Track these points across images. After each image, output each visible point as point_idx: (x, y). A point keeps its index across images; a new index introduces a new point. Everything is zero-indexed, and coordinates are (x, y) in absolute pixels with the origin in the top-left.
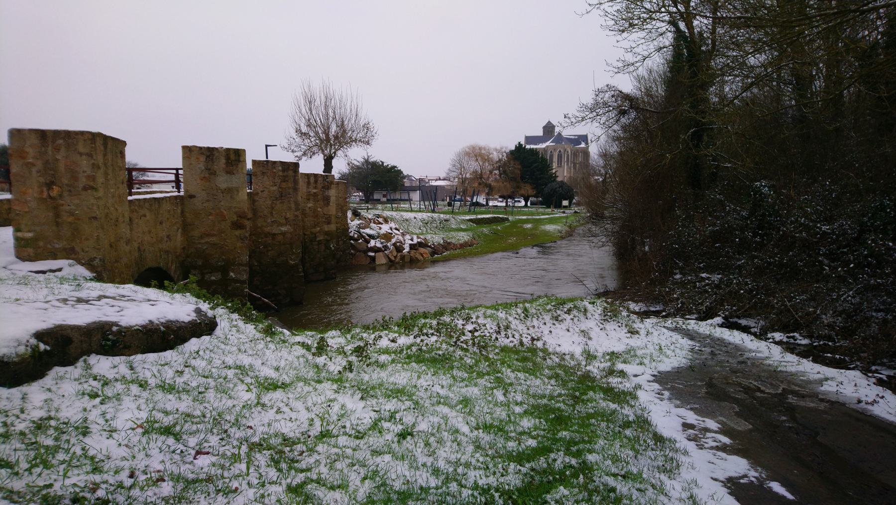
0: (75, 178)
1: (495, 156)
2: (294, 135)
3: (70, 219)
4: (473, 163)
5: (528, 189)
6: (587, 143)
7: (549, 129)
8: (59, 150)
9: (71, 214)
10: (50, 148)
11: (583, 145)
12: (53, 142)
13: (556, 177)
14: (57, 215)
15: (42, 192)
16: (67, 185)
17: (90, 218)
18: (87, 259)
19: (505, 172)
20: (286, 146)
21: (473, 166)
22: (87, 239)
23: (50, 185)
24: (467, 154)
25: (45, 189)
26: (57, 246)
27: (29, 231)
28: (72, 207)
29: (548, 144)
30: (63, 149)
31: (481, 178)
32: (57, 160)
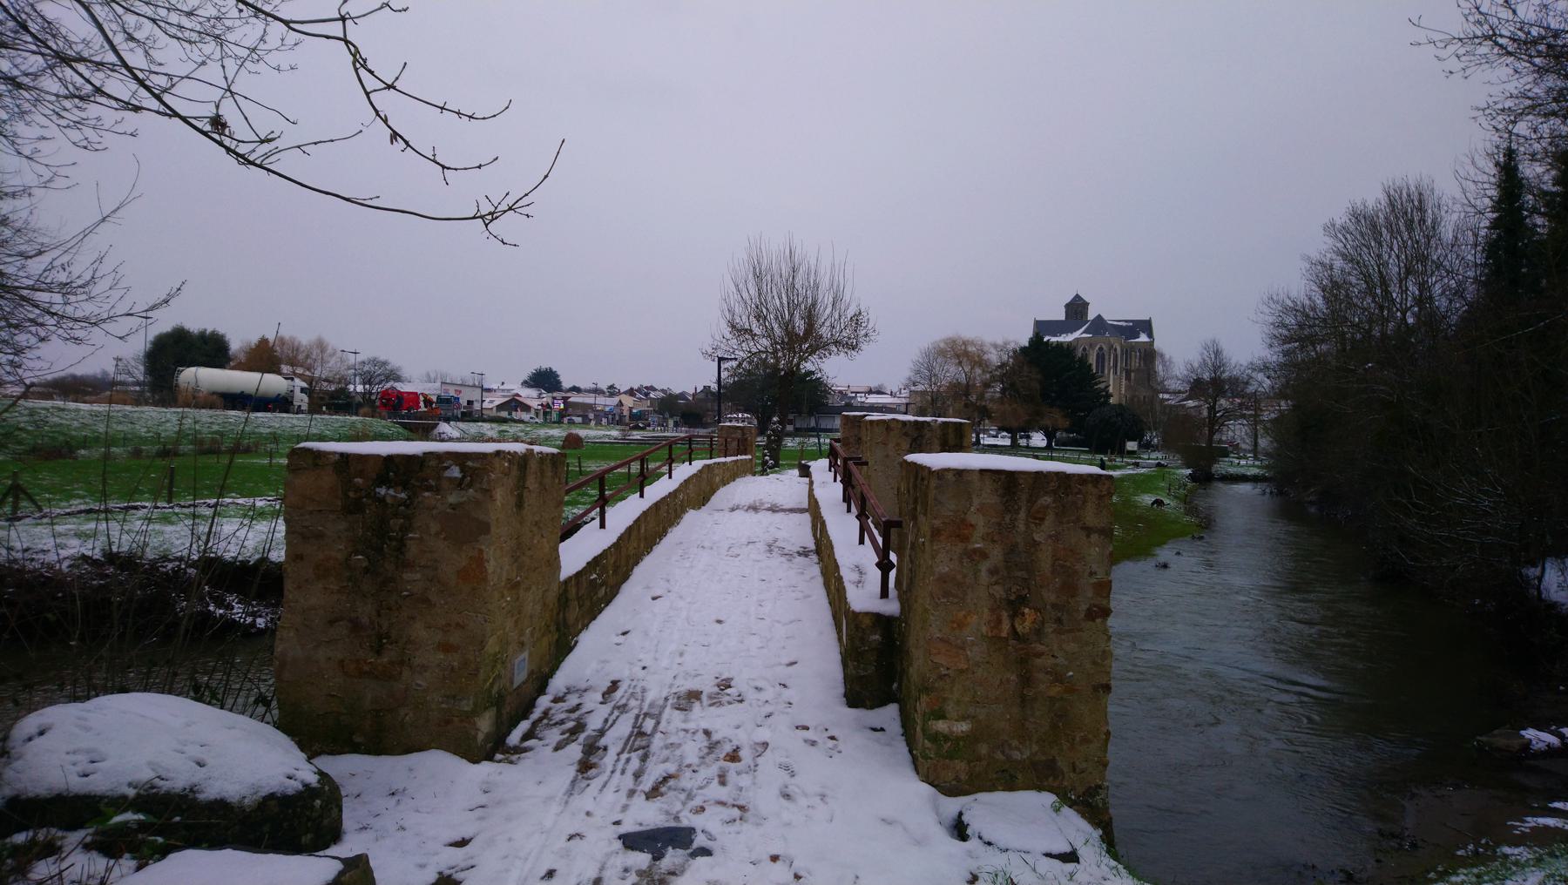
0: (1070, 589)
1: (994, 358)
2: (727, 331)
3: (1055, 690)
4: (953, 369)
5: (1056, 417)
6: (1150, 335)
7: (1077, 308)
8: (1042, 519)
9: (1058, 678)
10: (1022, 515)
11: (1143, 338)
12: (1032, 501)
13: (1109, 396)
14: (1026, 680)
15: (999, 621)
16: (1054, 606)
17: (1095, 689)
18: (1081, 790)
19: (1012, 385)
20: (710, 351)
21: (952, 372)
22: (1085, 740)
23: (1015, 606)
24: (941, 353)
25: (1005, 615)
26: (1016, 755)
27: (963, 718)
28: (1061, 660)
29: (1077, 334)
30: (1050, 519)
31: (967, 394)
32: (1036, 544)
